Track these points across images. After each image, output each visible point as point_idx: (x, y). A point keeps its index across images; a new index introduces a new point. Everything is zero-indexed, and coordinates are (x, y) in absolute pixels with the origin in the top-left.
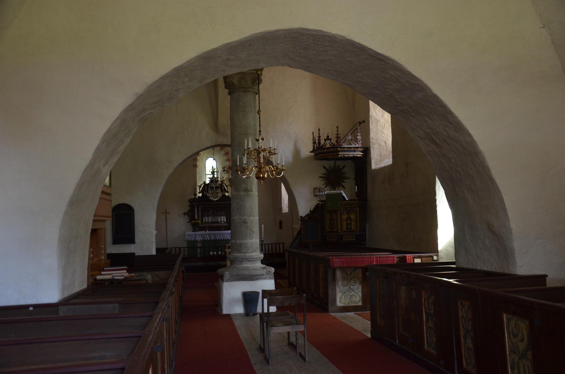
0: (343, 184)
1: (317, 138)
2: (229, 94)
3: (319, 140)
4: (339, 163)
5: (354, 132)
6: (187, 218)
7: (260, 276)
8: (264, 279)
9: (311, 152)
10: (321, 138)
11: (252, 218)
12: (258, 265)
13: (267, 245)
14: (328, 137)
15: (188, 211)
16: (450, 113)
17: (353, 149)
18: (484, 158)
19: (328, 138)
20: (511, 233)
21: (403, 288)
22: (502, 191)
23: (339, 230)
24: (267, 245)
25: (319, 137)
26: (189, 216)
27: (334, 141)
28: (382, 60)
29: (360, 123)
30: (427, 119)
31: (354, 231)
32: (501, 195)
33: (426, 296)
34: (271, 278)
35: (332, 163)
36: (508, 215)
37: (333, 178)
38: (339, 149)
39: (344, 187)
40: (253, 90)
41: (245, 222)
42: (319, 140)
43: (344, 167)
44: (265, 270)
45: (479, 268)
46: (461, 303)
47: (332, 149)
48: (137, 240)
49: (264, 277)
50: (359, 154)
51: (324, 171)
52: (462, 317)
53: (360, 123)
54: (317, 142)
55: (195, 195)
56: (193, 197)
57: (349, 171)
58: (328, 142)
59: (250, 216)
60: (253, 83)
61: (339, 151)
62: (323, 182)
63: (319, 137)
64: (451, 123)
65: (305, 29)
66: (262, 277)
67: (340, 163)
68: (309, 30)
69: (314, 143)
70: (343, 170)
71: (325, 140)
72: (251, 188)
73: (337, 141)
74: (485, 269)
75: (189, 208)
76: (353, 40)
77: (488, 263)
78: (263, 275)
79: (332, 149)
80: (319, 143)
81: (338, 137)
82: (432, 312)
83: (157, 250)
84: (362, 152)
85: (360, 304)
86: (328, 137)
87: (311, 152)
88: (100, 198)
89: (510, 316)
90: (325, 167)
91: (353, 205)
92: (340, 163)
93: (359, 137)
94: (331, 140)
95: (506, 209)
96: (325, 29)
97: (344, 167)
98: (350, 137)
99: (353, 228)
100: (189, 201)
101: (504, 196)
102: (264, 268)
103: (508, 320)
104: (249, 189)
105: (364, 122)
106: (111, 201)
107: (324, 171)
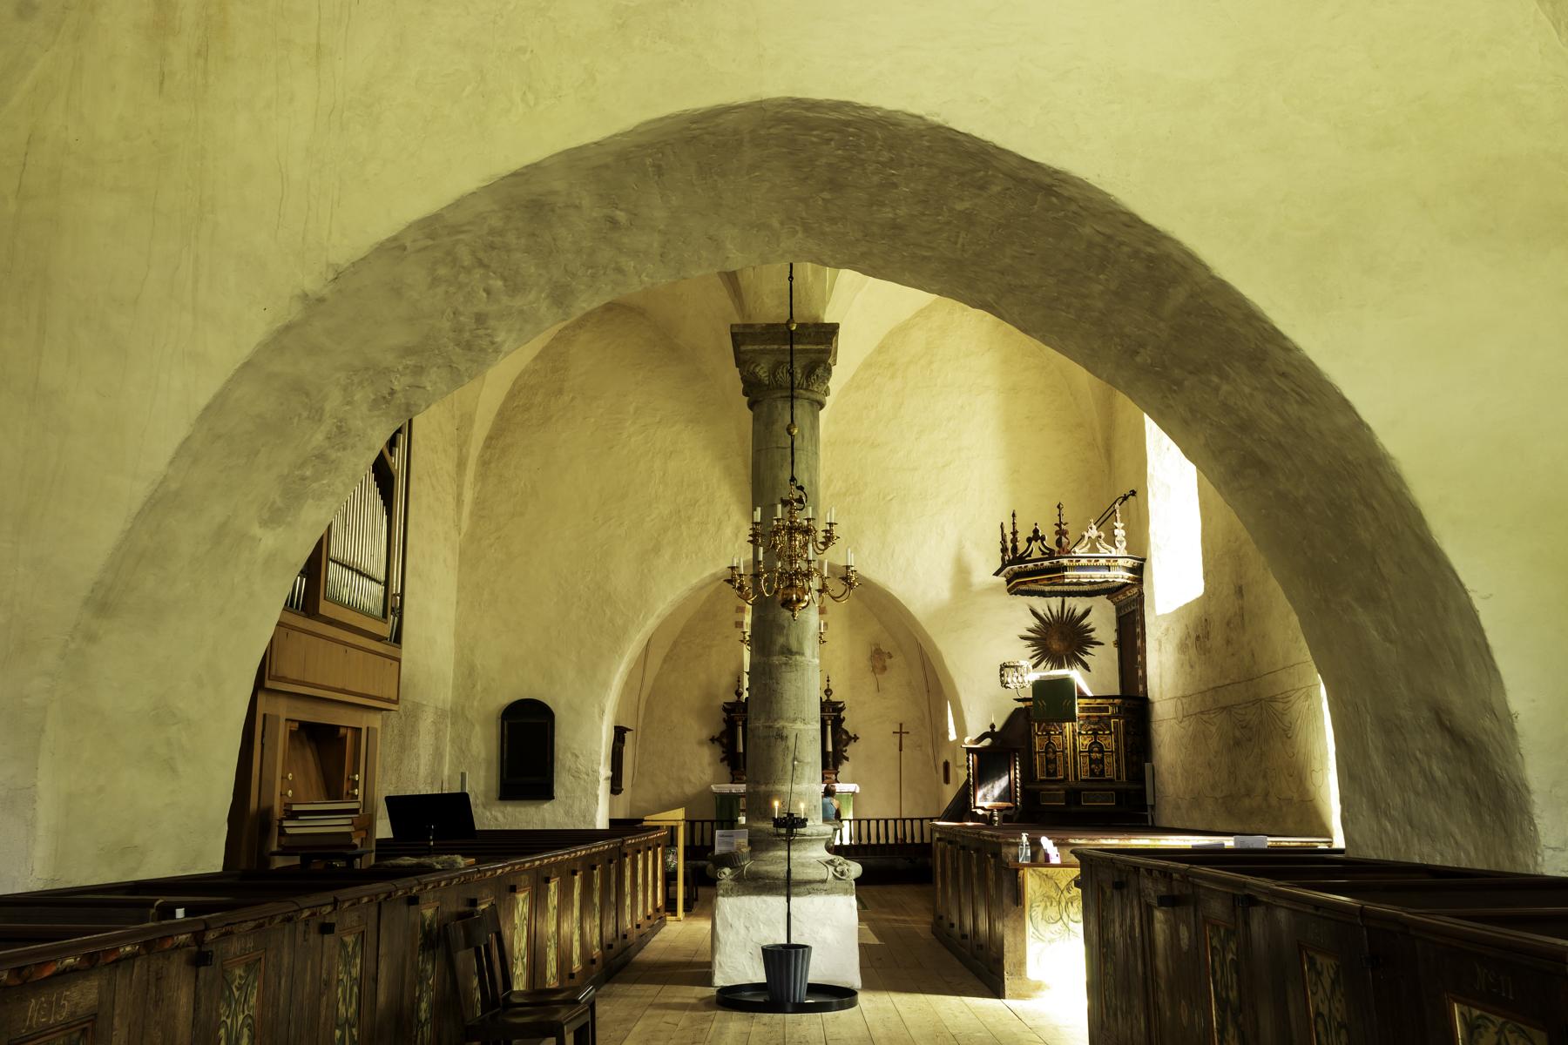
0: (1085, 658)
1: (1009, 537)
2: (751, 406)
3: (1014, 541)
4: (1071, 602)
5: (1105, 520)
6: (718, 750)
7: (816, 886)
8: (828, 892)
9: (997, 574)
10: (1019, 536)
11: (799, 725)
12: (815, 854)
13: (908, 823)
14: (1036, 531)
15: (722, 733)
16: (1275, 337)
17: (1103, 562)
18: (1398, 477)
19: (1036, 536)
20: (1513, 731)
21: (1159, 915)
22: (1468, 587)
23: (1071, 778)
24: (908, 823)
25: (1014, 533)
26: (722, 745)
27: (1050, 542)
28: (1049, 190)
29: (1125, 498)
30: (1215, 379)
31: (1111, 781)
32: (1469, 599)
33: (1215, 942)
34: (846, 892)
35: (1048, 606)
36: (1496, 670)
37: (1061, 639)
38: (1065, 561)
39: (1086, 666)
40: (809, 394)
41: (781, 737)
42: (1014, 541)
43: (1087, 613)
44: (831, 869)
45: (1417, 860)
46: (1312, 963)
47: (1046, 563)
48: (558, 791)
49: (827, 886)
50: (1120, 576)
51: (1033, 622)
52: (1319, 1014)
53: (1125, 498)
54: (1010, 545)
55: (739, 694)
56: (733, 698)
57: (1101, 619)
58: (1035, 545)
59: (794, 720)
60: (808, 377)
61: (1065, 568)
62: (1030, 652)
63: (1014, 533)
64: (1283, 375)
65: (799, 101)
66: (821, 886)
67: (1078, 605)
68: (814, 105)
69: (1004, 550)
70: (1085, 622)
71: (1029, 540)
72: (800, 643)
73: (1059, 543)
74: (1438, 861)
75: (723, 727)
76: (951, 125)
77: (1454, 846)
78: (824, 881)
79: (1046, 563)
80: (1015, 549)
81: (1061, 533)
82: (1233, 995)
83: (612, 822)
84: (1131, 570)
85: (391, 836)
86: (1036, 531)
87: (997, 574)
88: (280, 624)
89: (1476, 1012)
90: (1035, 614)
91: (1106, 710)
92: (1078, 605)
93: (1120, 533)
94: (1043, 539)
95: (1487, 646)
96: (861, 99)
97: (1087, 613)
98: (1094, 533)
99: (1110, 773)
100: (725, 709)
101: (1478, 604)
102: (831, 862)
103: (1472, 1028)
104: (794, 647)
105: (1133, 493)
106: (399, 661)
107: (1033, 622)
